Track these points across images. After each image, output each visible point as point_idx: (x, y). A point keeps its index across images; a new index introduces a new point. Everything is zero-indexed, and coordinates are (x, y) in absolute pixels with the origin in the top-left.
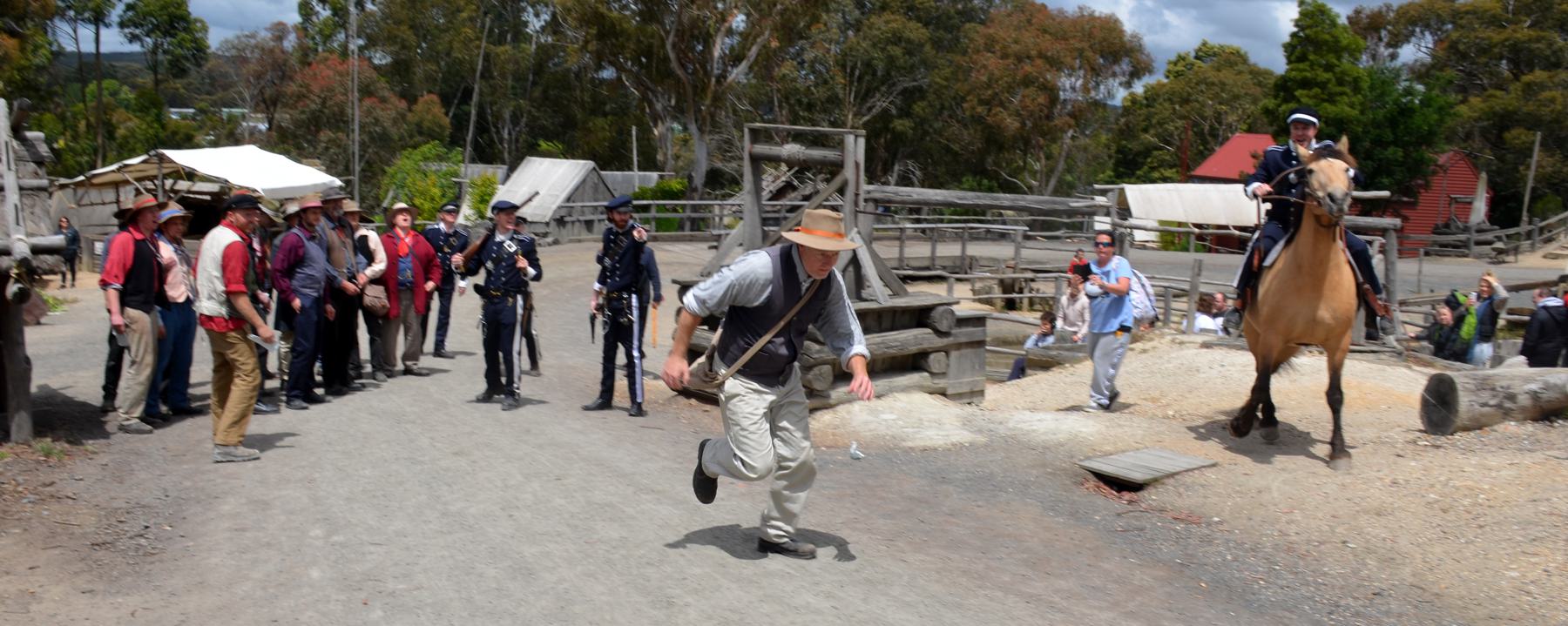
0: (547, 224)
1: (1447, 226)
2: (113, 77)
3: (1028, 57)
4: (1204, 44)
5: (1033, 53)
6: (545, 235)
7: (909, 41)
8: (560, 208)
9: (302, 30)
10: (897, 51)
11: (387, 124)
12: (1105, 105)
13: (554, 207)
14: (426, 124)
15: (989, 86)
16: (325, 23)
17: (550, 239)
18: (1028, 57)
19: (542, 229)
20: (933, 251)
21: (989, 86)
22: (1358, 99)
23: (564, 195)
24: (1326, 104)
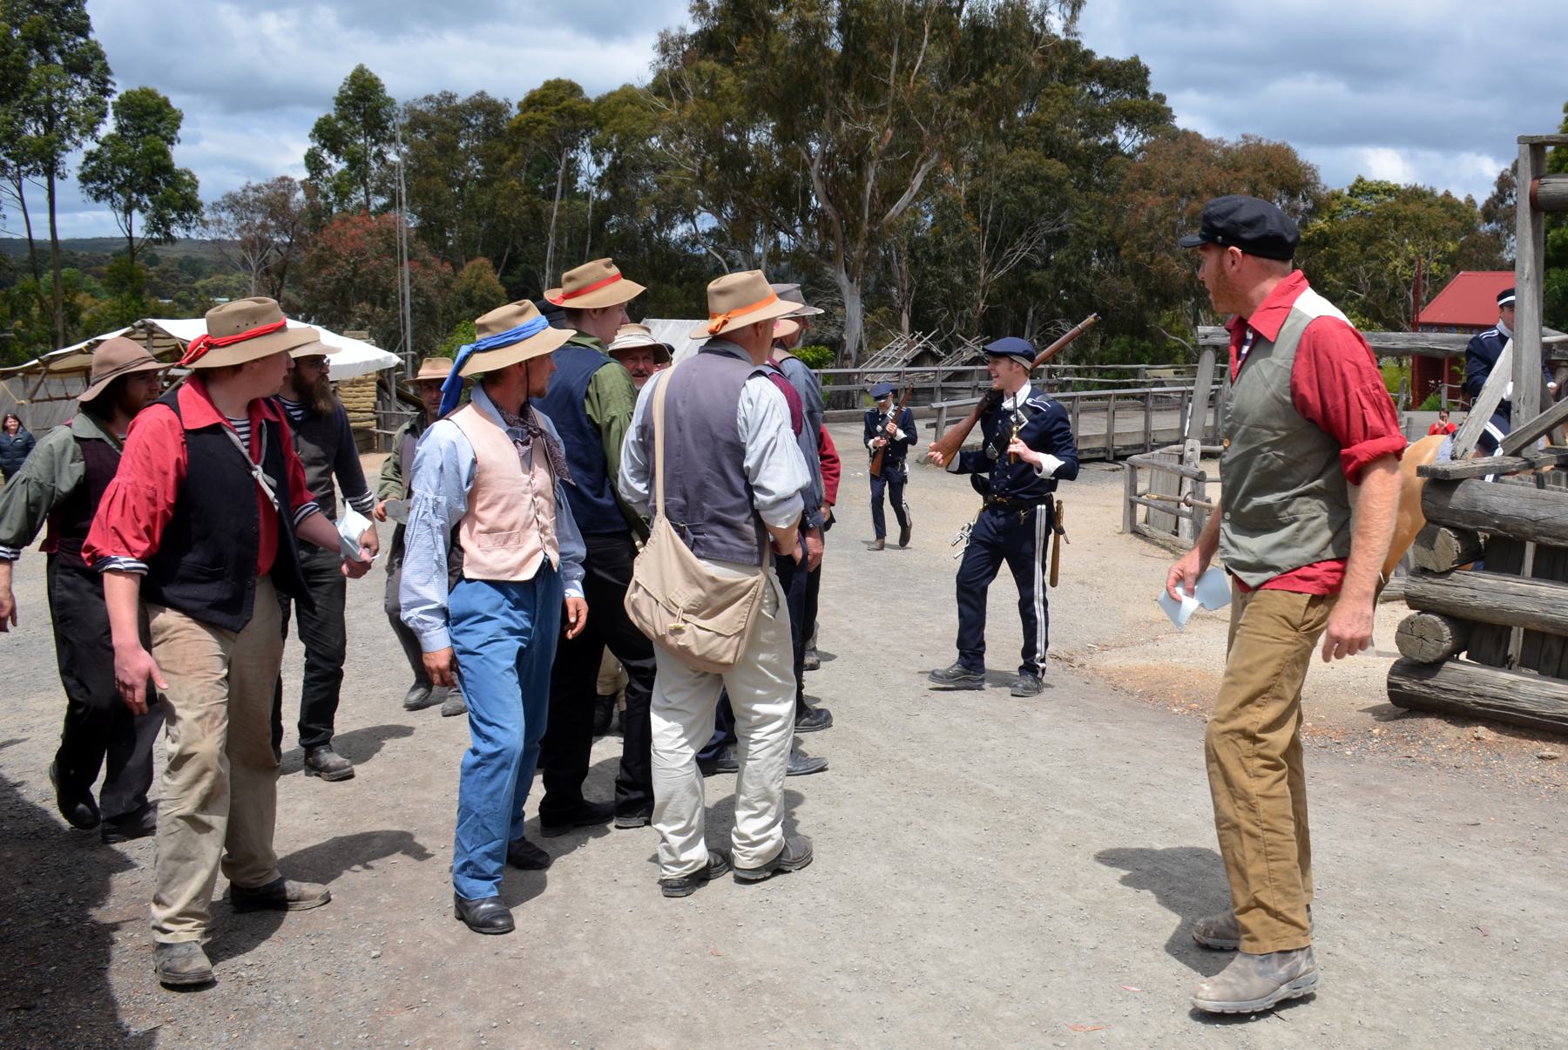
2: (73, 265)
3: (1193, 192)
4: (1361, 180)
5: (1199, 188)
7: (1047, 179)
9: (310, 188)
10: (1032, 191)
11: (433, 292)
14: (477, 293)
15: (1150, 227)
16: (341, 175)
18: (1193, 192)
20: (1111, 426)
21: (1150, 227)
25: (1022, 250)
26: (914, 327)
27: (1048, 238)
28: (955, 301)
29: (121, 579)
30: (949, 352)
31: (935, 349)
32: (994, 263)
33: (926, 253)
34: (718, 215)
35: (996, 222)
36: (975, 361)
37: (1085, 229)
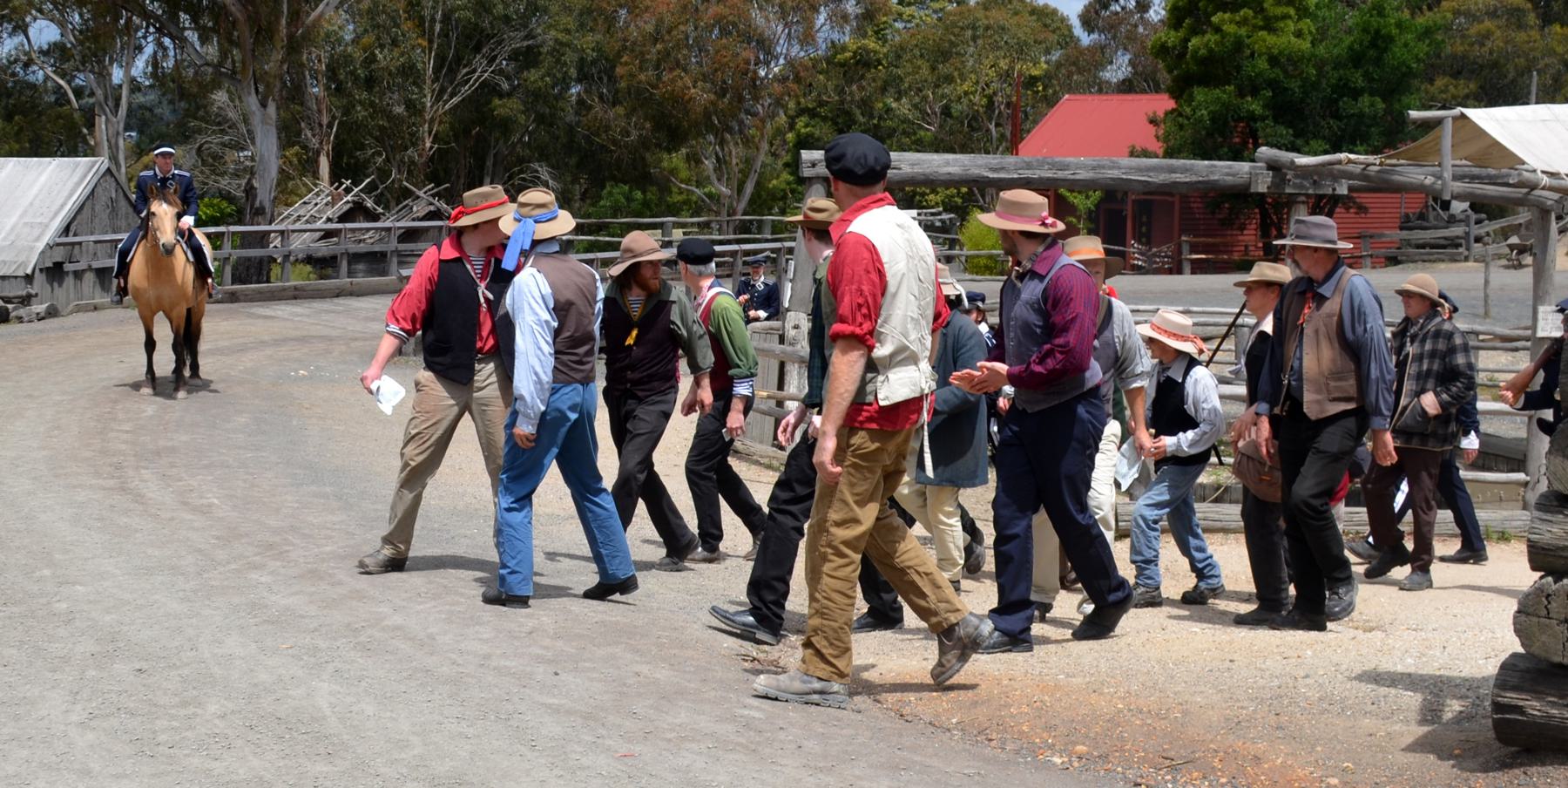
0: (29, 278)
1: (1422, 217)
6: (26, 300)
8: (50, 247)
12: (1246, 490)
13: (41, 246)
17: (39, 308)
19: (20, 290)
22: (1307, 24)
23: (57, 223)
24: (1263, 33)
25: (481, 70)
26: (335, 178)
27: (514, 56)
28: (395, 136)
29: (1479, 280)
30: (387, 208)
31: (369, 204)
32: (442, 91)
33: (352, 73)
34: (61, 24)
35: (445, 34)
36: (430, 216)
37: (561, 44)
